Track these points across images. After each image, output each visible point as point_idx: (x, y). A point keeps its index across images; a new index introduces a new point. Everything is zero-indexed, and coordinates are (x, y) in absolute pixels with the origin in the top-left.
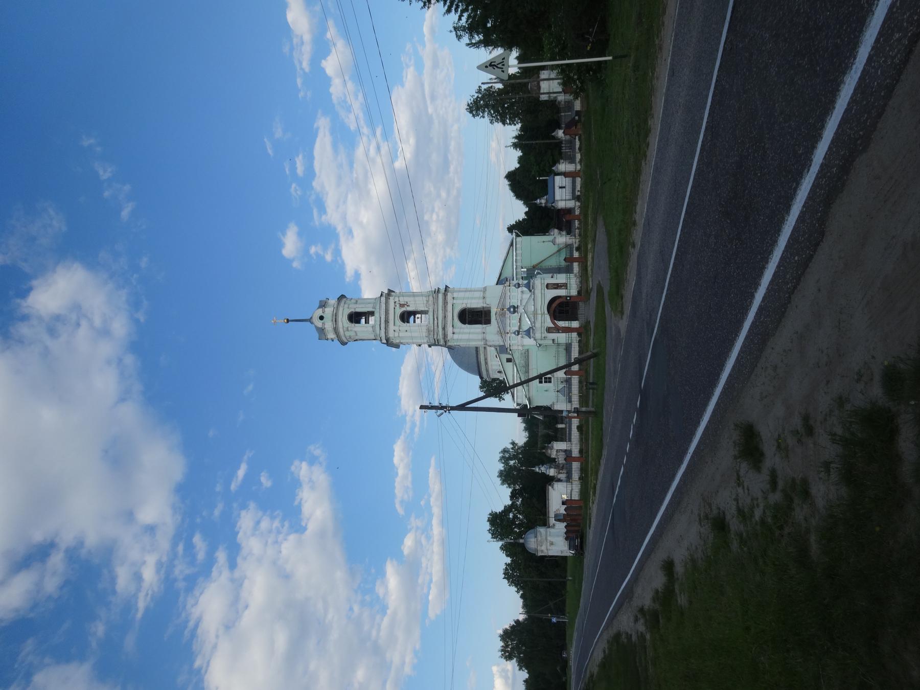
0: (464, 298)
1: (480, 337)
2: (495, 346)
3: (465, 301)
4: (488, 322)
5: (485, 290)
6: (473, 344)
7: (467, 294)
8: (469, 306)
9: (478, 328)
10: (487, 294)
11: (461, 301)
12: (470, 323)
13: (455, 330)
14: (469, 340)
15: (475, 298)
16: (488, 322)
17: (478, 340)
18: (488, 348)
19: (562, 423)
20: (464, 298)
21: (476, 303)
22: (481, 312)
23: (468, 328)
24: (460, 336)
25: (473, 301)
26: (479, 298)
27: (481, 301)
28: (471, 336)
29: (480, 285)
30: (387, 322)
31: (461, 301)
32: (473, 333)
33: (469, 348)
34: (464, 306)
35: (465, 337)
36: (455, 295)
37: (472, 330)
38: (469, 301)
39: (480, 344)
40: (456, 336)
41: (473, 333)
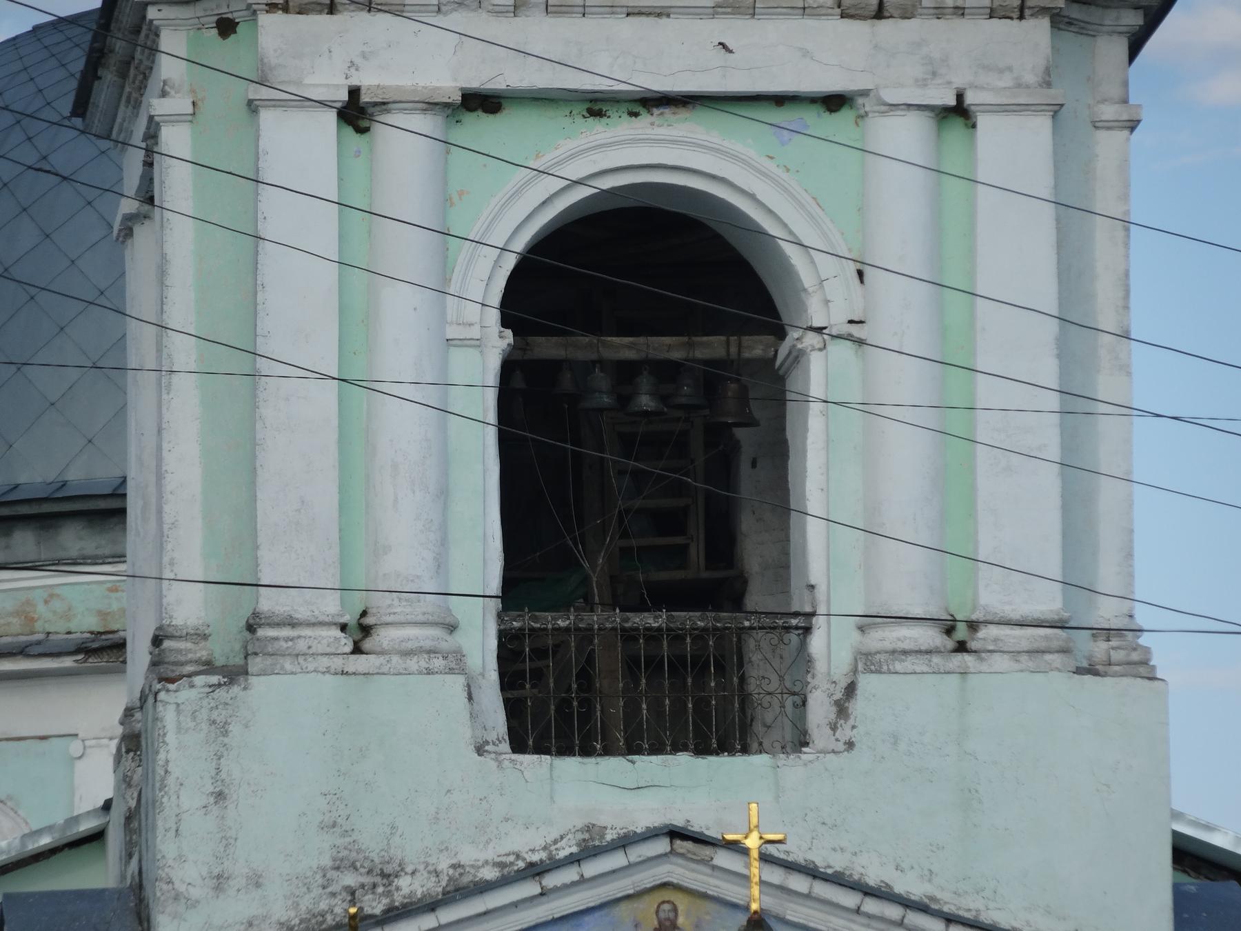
0: (948, 286)
1: (300, 570)
2: (133, 816)
3: (899, 312)
4: (550, 704)
5: (1098, 648)
6: (174, 453)
7: (1017, 348)
8: (823, 373)
9: (439, 518)
10: (1014, 697)
11: (899, 234)
12: (532, 408)
13: (403, 145)
14: (242, 362)
15: (952, 488)
16: (550, 704)
17: (240, 523)
18: (97, 709)
19: (647, 684)
20: (948, 286)
21: (865, 495)
22: (726, 590)
23: (441, 364)
24: (299, 224)
25: (906, 455)
26: (953, 552)
27: (908, 584)
28: (300, 420)
29: (1162, 568)
30: (596, 105)
31: (899, 234)
32: (353, 447)
33: (110, 368)
34: (820, 290)
35: (299, 307)
36: (1012, 147)
37: (402, 428)
38: (902, 381)
39: (175, 573)
40: (302, 146)
41: (353, 447)
